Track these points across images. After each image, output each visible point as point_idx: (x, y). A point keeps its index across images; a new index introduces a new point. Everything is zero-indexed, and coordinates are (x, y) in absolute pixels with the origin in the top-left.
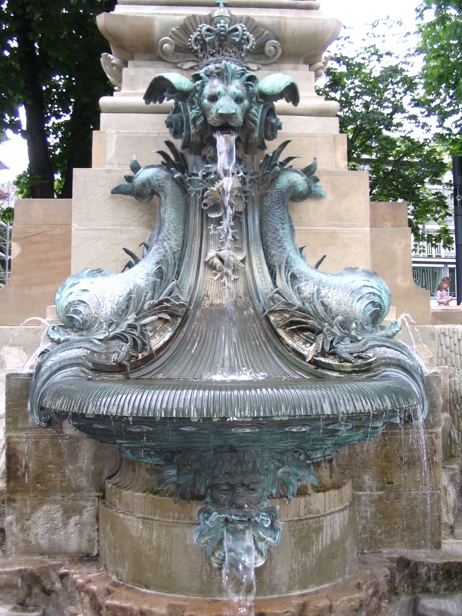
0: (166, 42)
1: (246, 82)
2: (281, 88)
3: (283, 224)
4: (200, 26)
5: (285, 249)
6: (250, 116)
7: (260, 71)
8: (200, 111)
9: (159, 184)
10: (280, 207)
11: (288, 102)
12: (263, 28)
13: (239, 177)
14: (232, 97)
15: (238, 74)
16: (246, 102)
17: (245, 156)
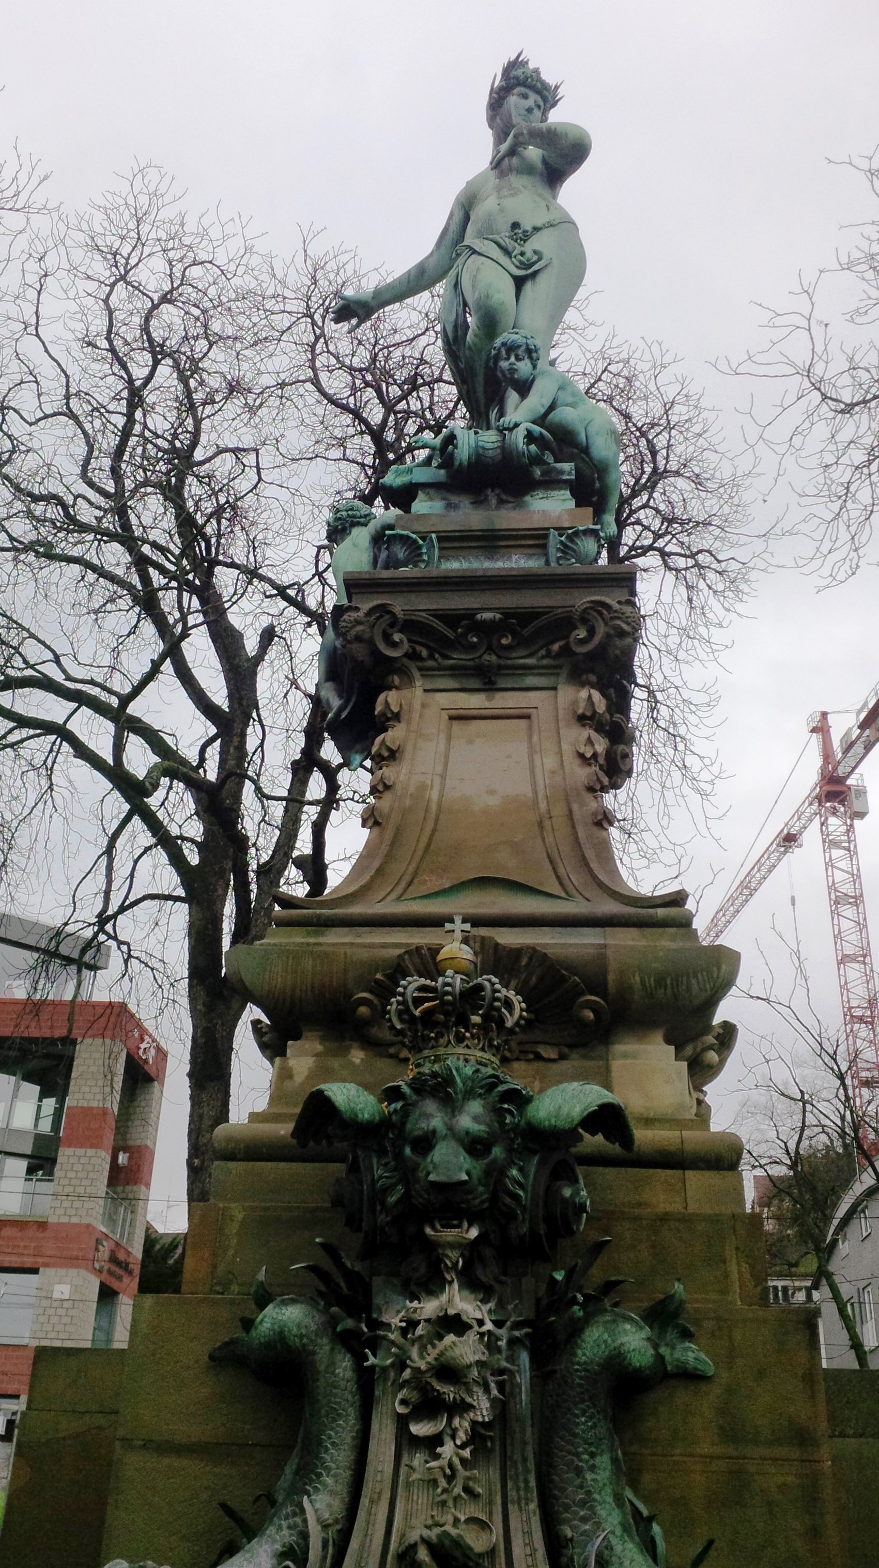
0: (363, 1002)
1: (499, 1105)
2: (573, 1120)
3: (592, 1455)
4: (403, 982)
5: (598, 1524)
6: (505, 1185)
7: (565, 1062)
8: (395, 1174)
9: (304, 1345)
10: (584, 1412)
11: (614, 1144)
12: (566, 969)
13: (482, 1335)
14: (460, 1141)
15: (481, 1087)
16: (497, 1152)
17: (503, 1278)
